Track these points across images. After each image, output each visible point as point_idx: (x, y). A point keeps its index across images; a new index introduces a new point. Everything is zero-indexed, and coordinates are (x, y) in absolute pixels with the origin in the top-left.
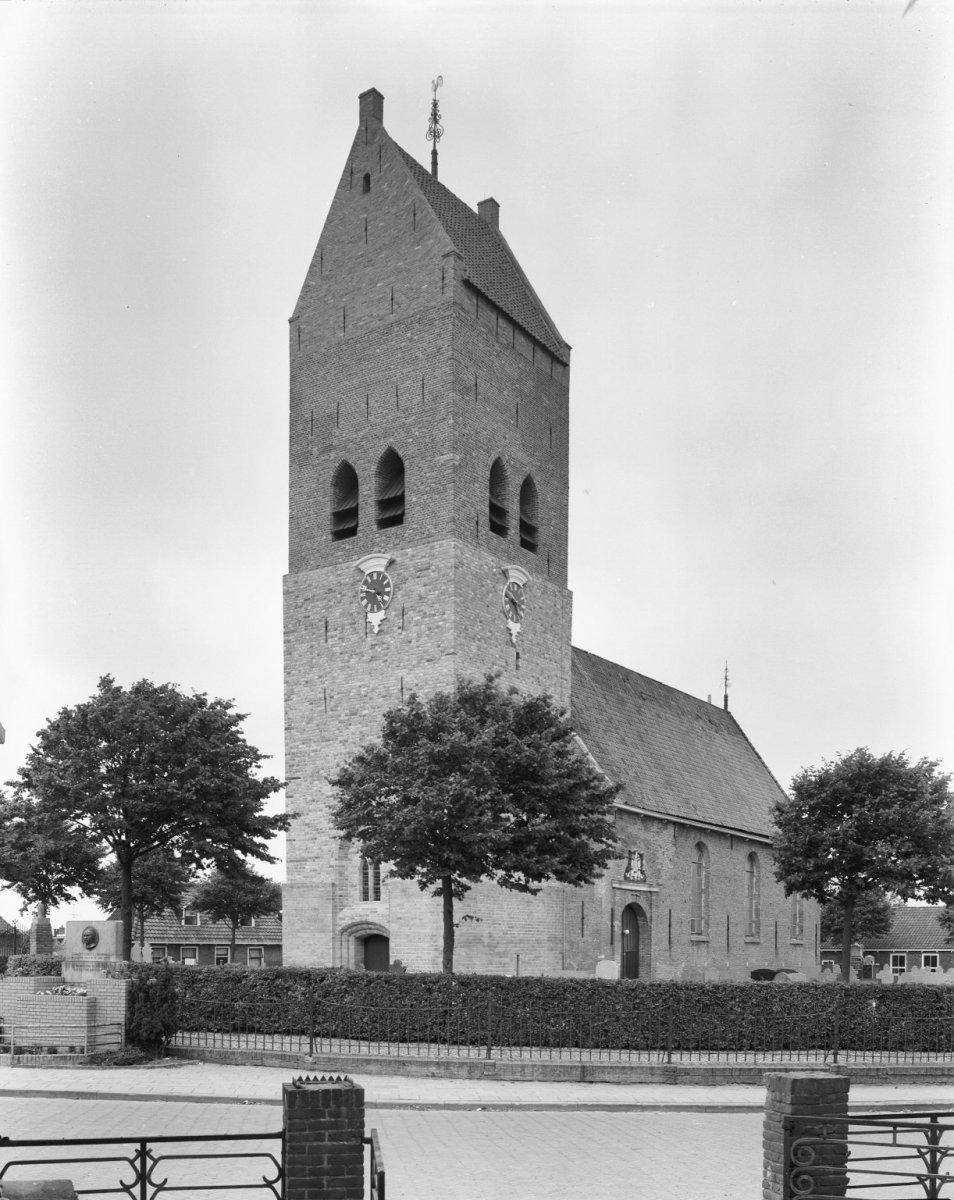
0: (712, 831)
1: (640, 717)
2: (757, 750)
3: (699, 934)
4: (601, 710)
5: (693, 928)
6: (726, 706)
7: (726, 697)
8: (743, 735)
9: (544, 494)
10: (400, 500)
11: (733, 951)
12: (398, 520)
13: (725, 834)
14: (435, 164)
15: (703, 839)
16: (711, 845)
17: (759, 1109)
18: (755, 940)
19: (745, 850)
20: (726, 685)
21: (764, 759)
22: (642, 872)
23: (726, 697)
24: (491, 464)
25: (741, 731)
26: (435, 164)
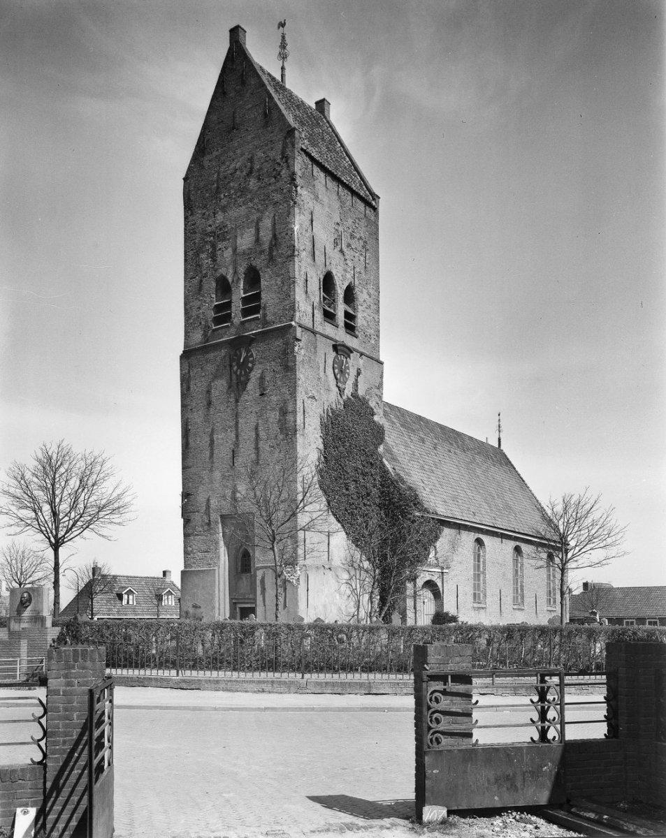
0: (471, 526)
1: (436, 452)
2: (522, 476)
3: (479, 603)
4: (407, 446)
5: (475, 598)
6: (499, 445)
7: (499, 439)
8: (512, 465)
9: (361, 296)
10: (257, 297)
11: (504, 615)
12: (256, 310)
13: (497, 533)
14: (283, 76)
15: (481, 536)
16: (486, 539)
17: (567, 704)
18: (520, 607)
19: (513, 544)
20: (499, 431)
21: (526, 482)
22: (437, 559)
23: (499, 439)
24: (345, 288)
25: (510, 462)
26: (283, 76)
